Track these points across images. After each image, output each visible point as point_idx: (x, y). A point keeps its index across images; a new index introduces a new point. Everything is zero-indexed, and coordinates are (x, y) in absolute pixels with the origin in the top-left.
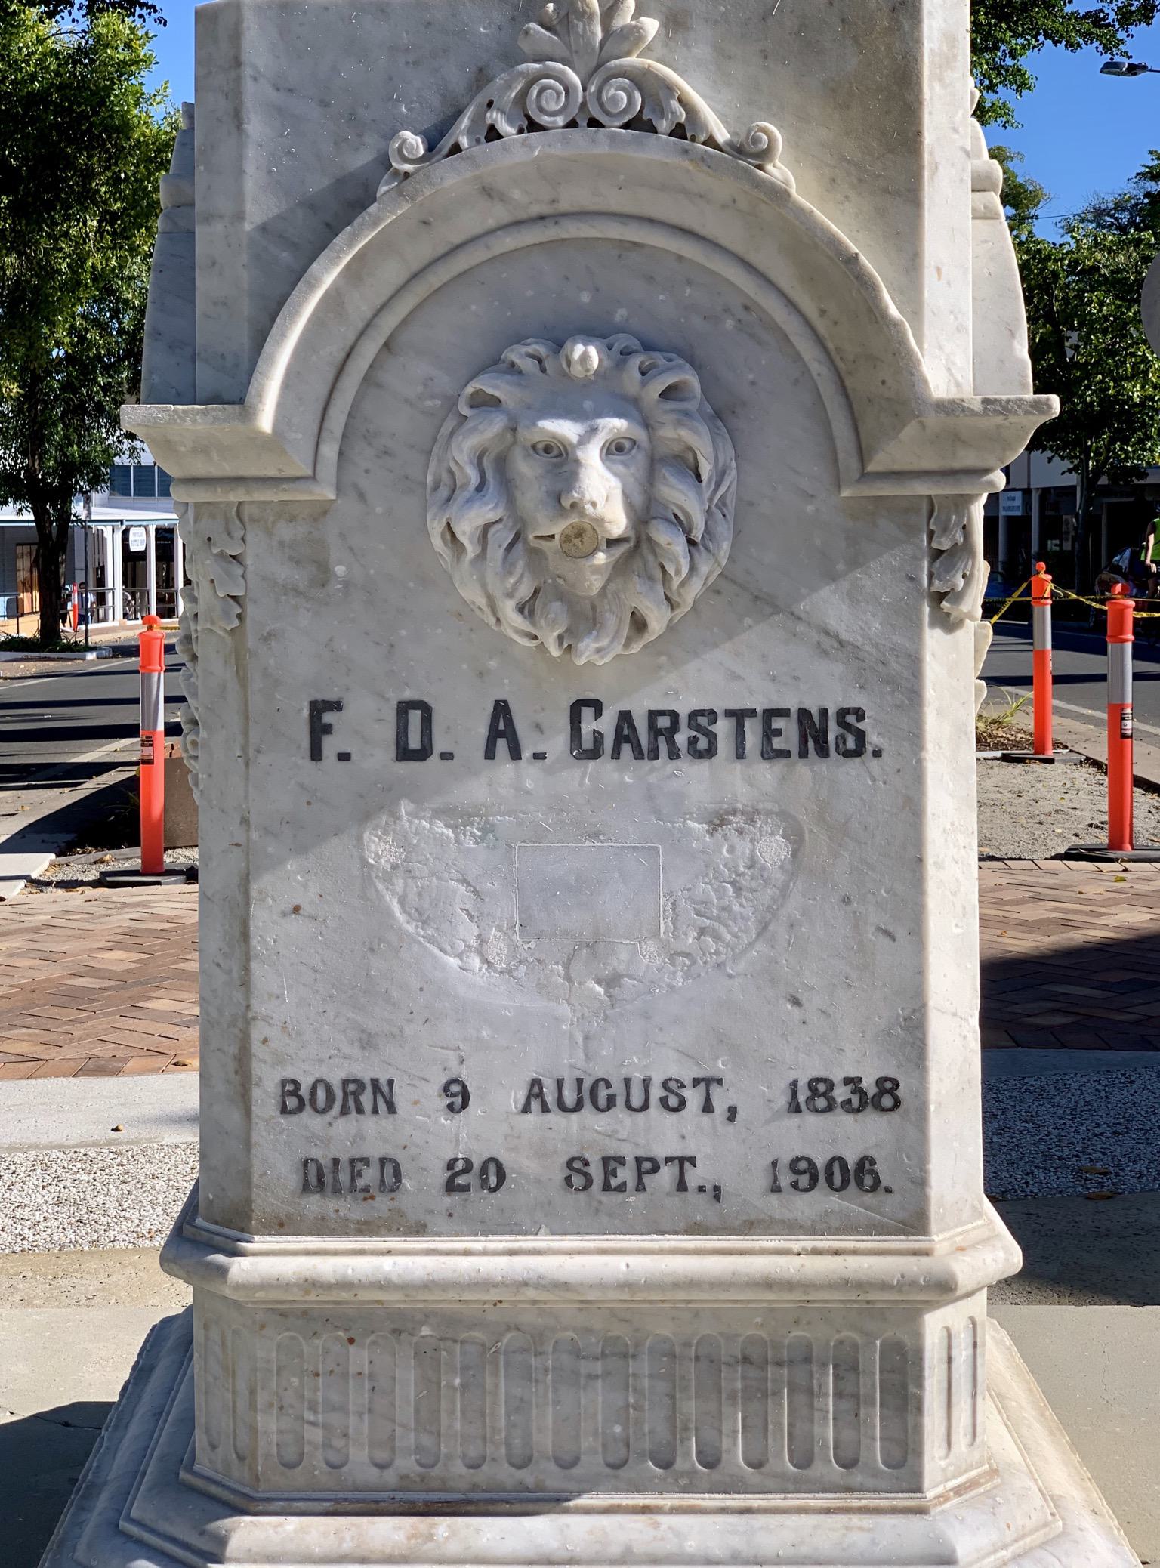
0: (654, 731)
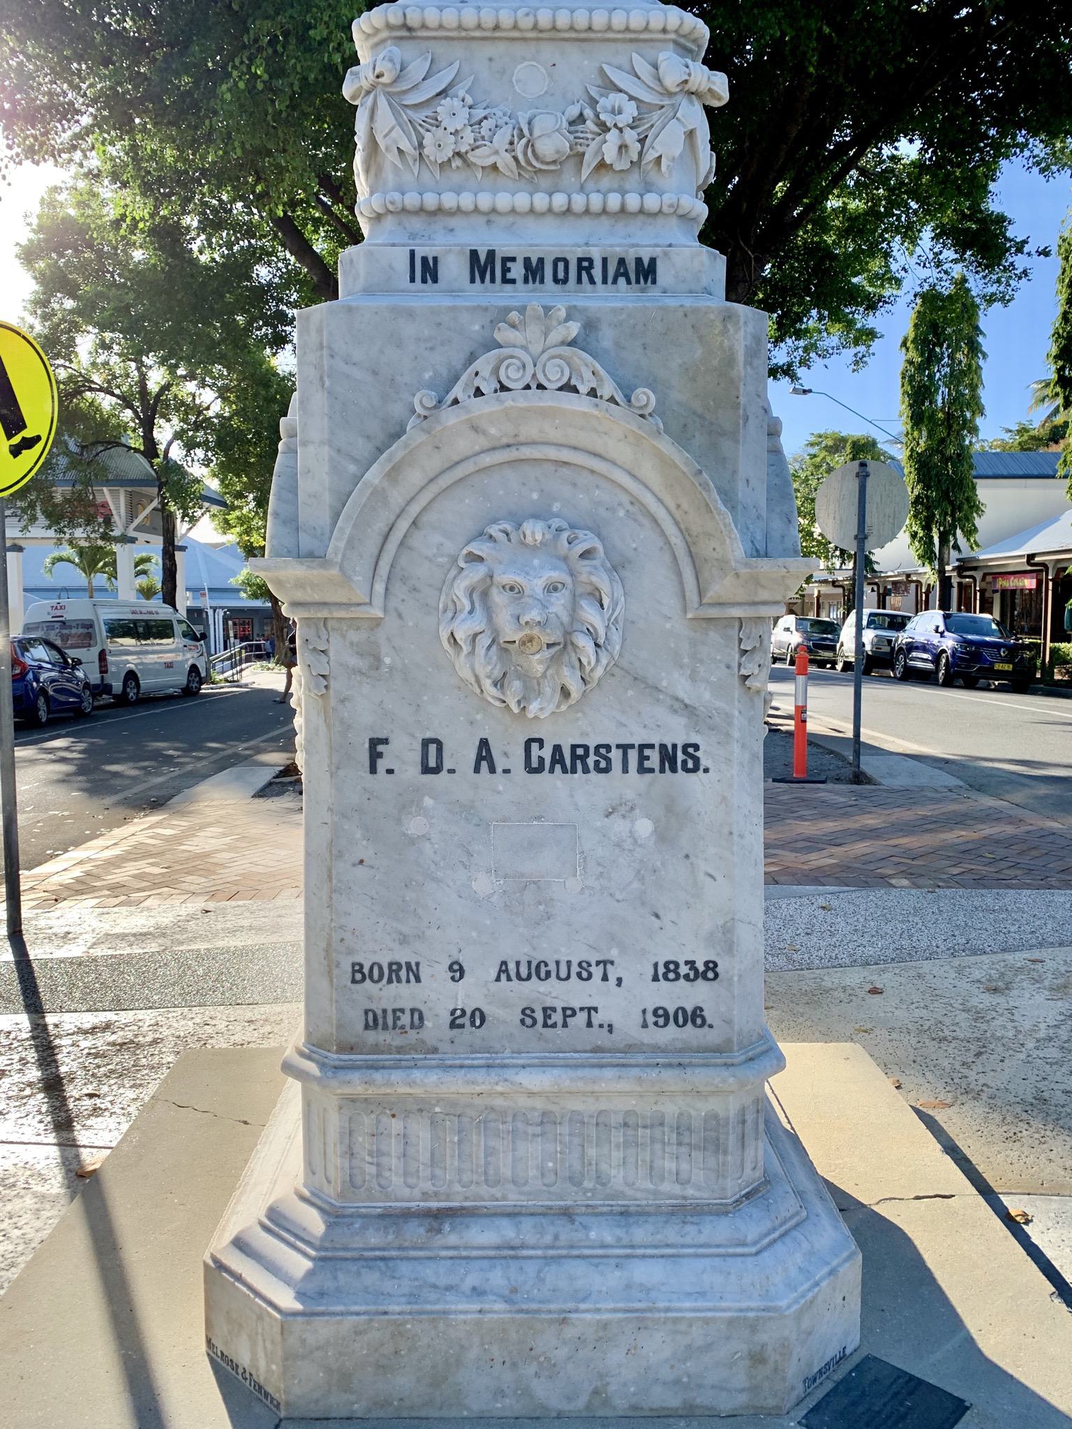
0: (574, 757)
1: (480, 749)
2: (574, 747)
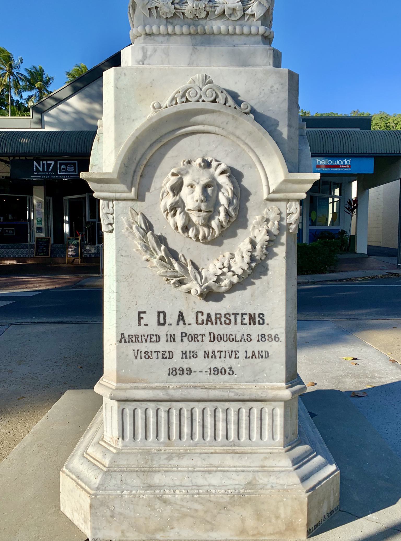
1: (179, 317)
2: (216, 315)
